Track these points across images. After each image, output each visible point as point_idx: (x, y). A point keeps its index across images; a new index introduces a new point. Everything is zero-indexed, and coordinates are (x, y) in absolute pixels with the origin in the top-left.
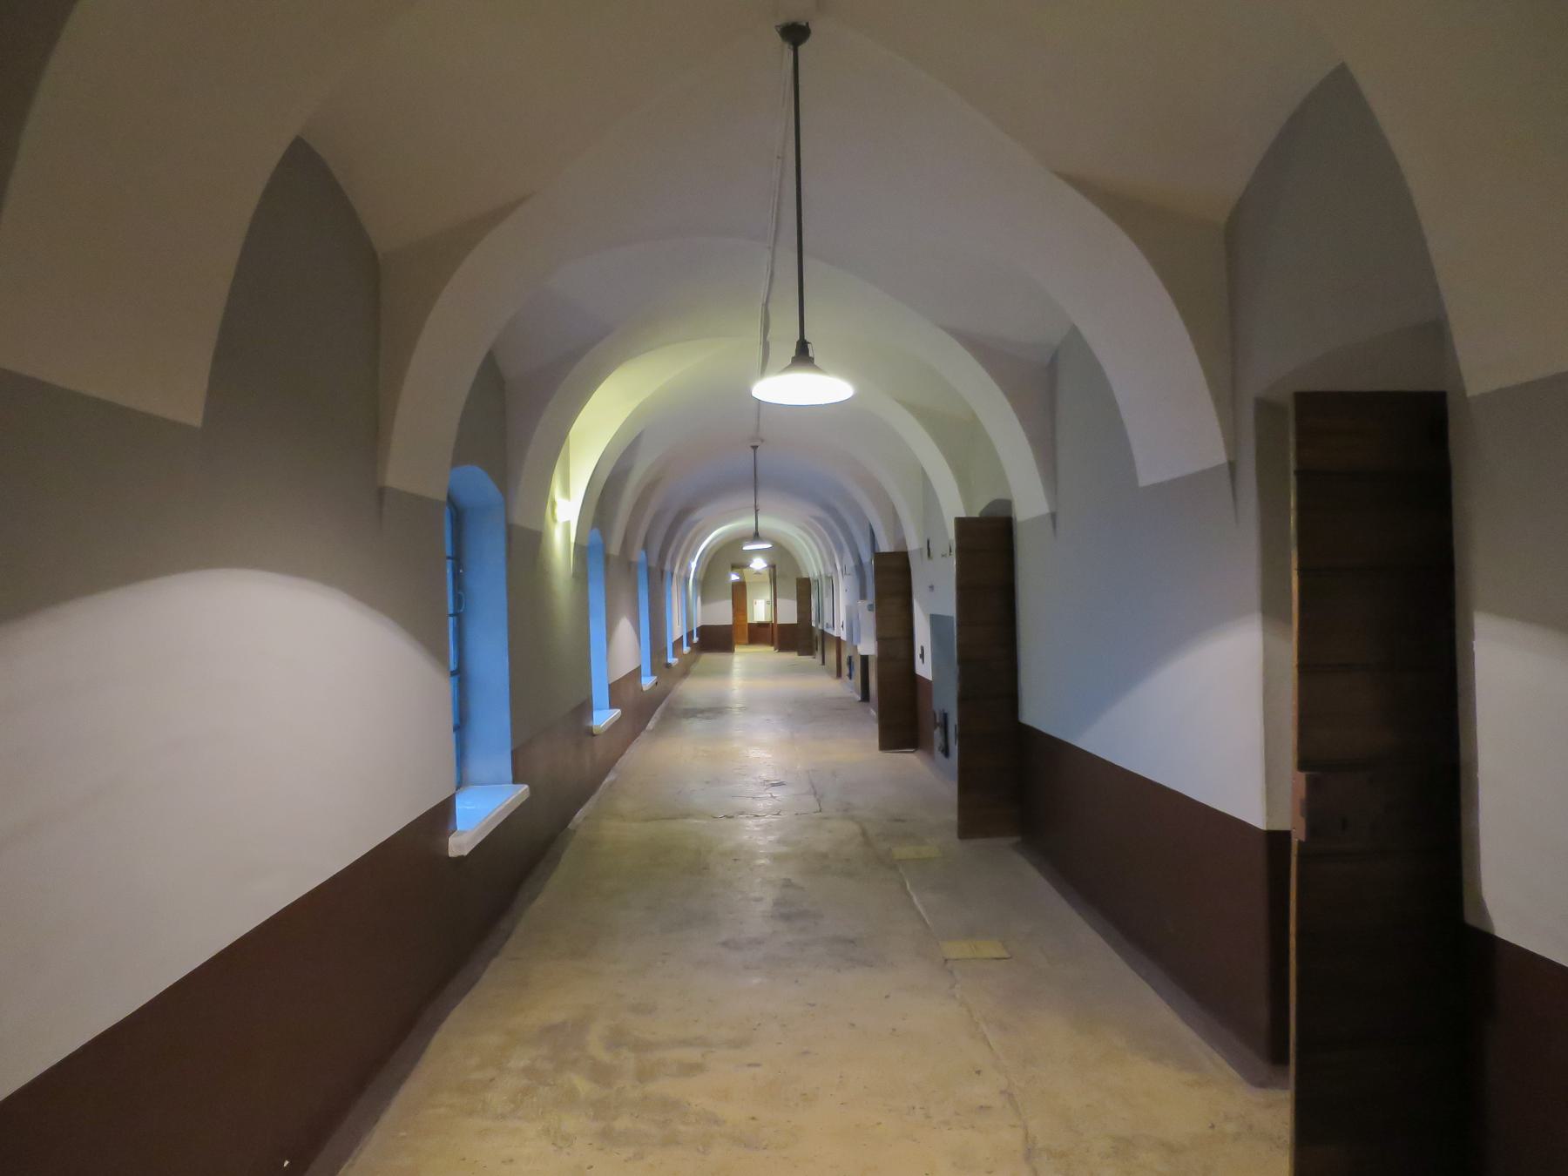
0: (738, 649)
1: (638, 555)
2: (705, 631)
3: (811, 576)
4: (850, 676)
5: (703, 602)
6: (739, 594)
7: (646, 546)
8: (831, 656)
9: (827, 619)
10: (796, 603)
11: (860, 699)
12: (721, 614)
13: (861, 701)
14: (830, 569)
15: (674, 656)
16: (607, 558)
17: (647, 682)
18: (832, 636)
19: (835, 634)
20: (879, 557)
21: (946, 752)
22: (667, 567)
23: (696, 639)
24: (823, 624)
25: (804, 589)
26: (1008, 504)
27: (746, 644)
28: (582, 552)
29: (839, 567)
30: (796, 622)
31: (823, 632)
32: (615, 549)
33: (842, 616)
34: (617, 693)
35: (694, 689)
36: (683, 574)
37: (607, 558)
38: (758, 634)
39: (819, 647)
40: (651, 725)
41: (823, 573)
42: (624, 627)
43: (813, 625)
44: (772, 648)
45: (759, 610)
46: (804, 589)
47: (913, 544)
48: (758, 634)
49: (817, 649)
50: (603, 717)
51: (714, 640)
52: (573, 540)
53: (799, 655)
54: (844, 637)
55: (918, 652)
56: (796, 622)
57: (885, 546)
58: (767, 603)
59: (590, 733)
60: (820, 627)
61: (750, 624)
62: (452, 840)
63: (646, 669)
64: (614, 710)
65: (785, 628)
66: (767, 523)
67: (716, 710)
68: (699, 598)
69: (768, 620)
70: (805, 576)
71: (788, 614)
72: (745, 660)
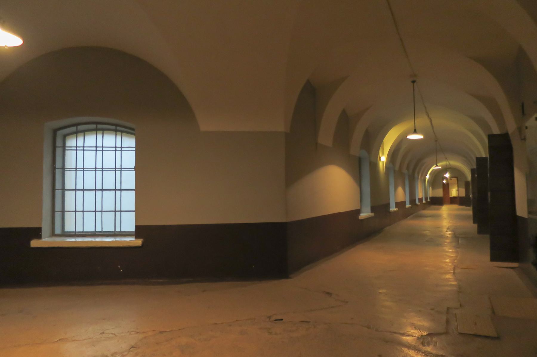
1: (405, 171)
2: (432, 199)
5: (433, 189)
6: (446, 188)
7: (408, 168)
12: (439, 193)
16: (395, 171)
17: (408, 206)
20: (491, 137)
22: (416, 175)
23: (429, 200)
28: (387, 168)
32: (397, 168)
34: (397, 204)
36: (423, 178)
37: (395, 171)
38: (453, 201)
40: (408, 218)
42: (400, 190)
45: (454, 193)
48: (453, 201)
50: (393, 209)
51: (436, 202)
52: (385, 165)
56: (465, 196)
57: (496, 131)
58: (456, 190)
59: (390, 212)
62: (360, 216)
65: (461, 198)
68: (431, 188)
69: (457, 196)
72: (445, 210)
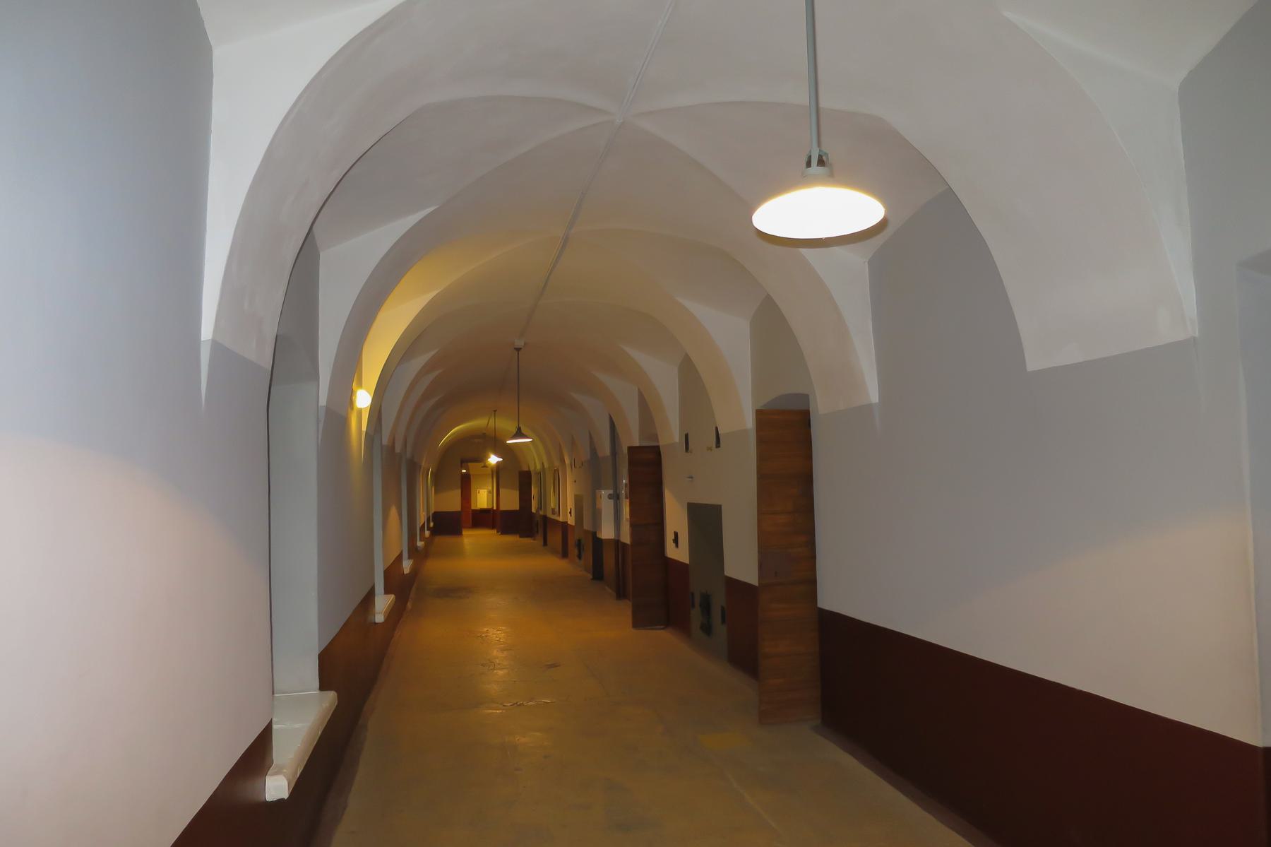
0: (465, 532)
3: (532, 469)
4: (579, 557)
5: (436, 492)
6: (466, 485)
8: (555, 538)
9: (552, 503)
10: (518, 492)
11: (591, 577)
12: (451, 501)
13: (593, 579)
14: (557, 463)
15: (421, 540)
17: (407, 566)
18: (558, 522)
19: (561, 519)
21: (707, 629)
23: (432, 524)
24: (545, 510)
25: (525, 481)
26: (805, 398)
27: (469, 528)
29: (567, 461)
30: (518, 509)
31: (545, 517)
33: (570, 504)
35: (438, 569)
38: (483, 519)
39: (541, 531)
40: (409, 605)
41: (546, 465)
43: (534, 510)
44: (494, 532)
45: (483, 498)
46: (525, 481)
47: (670, 434)
48: (483, 519)
49: (537, 532)
51: (447, 525)
52: (364, 429)
53: (520, 537)
54: (571, 521)
55: (669, 537)
56: (518, 509)
60: (541, 513)
61: (473, 510)
63: (405, 555)
64: (390, 596)
66: (504, 424)
67: (456, 591)
70: (525, 469)
71: (511, 501)
72: (472, 539)
